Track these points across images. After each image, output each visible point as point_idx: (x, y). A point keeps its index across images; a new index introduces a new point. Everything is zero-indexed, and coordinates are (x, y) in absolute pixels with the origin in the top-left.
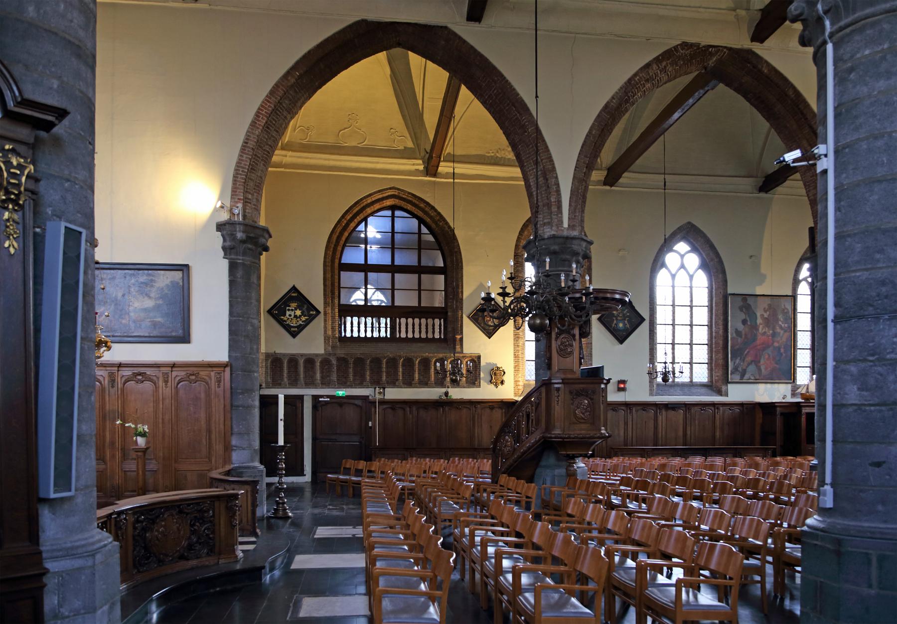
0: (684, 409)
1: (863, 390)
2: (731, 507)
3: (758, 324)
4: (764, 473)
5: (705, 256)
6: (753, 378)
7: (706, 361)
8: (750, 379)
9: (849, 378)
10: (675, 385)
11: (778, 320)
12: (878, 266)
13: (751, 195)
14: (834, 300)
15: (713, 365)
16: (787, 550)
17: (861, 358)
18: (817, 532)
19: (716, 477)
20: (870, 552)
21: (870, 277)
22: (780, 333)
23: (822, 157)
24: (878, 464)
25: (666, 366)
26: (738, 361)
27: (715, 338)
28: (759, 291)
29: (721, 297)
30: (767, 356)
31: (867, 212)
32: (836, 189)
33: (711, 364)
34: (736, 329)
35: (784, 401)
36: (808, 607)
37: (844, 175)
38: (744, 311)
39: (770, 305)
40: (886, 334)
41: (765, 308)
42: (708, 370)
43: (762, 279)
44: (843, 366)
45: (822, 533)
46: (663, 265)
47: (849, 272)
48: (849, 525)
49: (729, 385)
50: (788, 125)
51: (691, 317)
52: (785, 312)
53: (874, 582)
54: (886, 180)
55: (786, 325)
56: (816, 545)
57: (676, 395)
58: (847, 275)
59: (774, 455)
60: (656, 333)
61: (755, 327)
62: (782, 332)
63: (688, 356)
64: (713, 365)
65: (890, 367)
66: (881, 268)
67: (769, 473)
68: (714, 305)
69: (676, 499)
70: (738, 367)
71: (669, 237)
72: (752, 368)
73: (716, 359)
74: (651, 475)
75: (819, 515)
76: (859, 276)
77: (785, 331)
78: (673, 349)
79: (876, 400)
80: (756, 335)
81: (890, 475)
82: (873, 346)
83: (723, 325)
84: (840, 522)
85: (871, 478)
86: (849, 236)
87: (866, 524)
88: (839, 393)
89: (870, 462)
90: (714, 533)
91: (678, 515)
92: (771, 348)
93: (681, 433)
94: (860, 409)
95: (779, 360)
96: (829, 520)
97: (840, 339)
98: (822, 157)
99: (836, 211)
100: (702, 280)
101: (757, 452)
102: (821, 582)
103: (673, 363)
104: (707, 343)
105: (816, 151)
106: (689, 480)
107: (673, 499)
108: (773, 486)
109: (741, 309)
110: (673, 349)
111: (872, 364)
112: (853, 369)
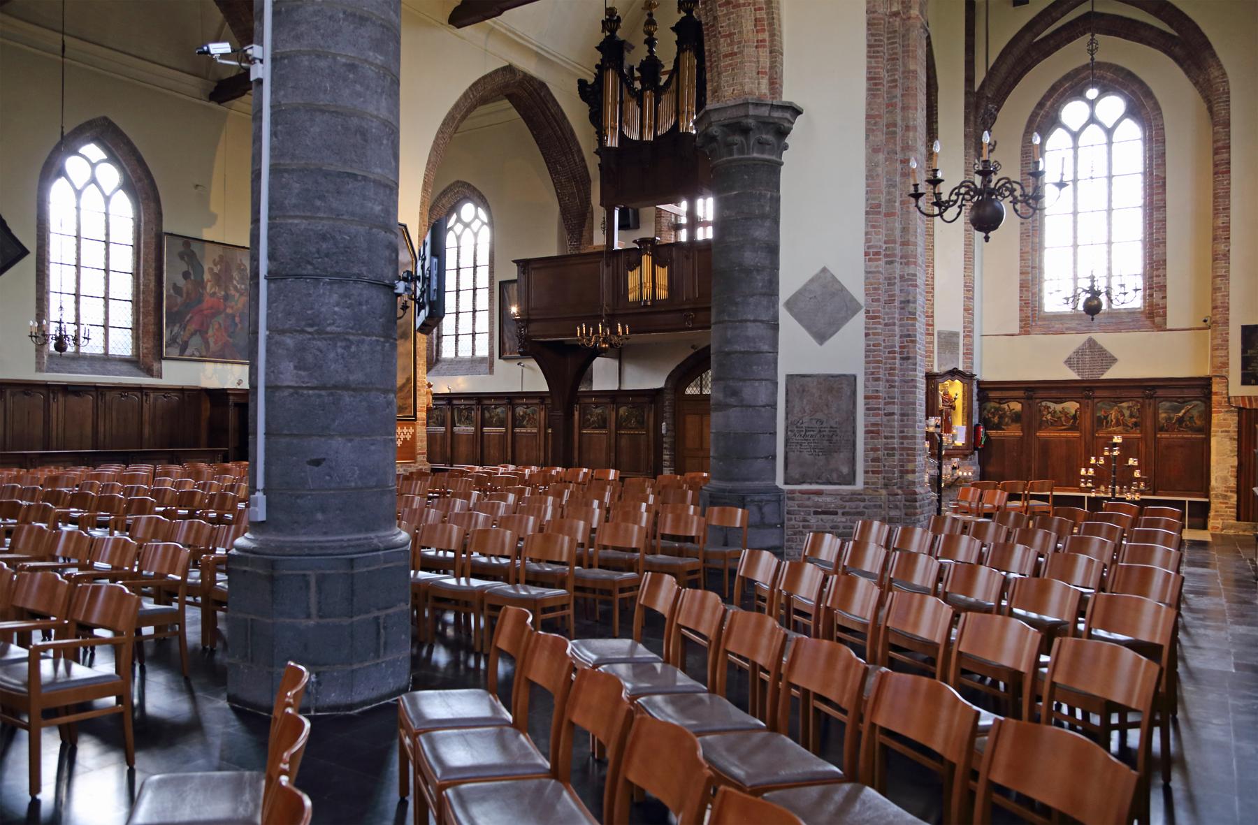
0: (94, 394)
1: (300, 369)
2: (187, 537)
3: (205, 280)
4: (205, 484)
5: (130, 174)
6: (197, 354)
7: (130, 326)
8: (193, 355)
9: (285, 352)
10: (78, 357)
11: (231, 278)
12: (318, 215)
13: (198, 101)
14: (268, 250)
15: (141, 332)
16: (218, 584)
17: (299, 329)
18: (247, 554)
19: (134, 492)
20: (308, 572)
21: (310, 227)
22: (234, 296)
23: (257, 61)
24: (317, 463)
25: (61, 328)
26: (176, 329)
27: (143, 293)
28: (207, 235)
29: (153, 235)
30: (217, 326)
31: (307, 145)
32: (272, 107)
33: (137, 330)
34: (175, 284)
35: (239, 387)
36: (237, 656)
37: (282, 93)
38: (186, 258)
39: (221, 257)
40: (327, 301)
41: (214, 260)
42: (133, 338)
43: (211, 220)
44: (277, 337)
45: (252, 556)
46: (61, 173)
47: (284, 217)
48: (284, 542)
49: (164, 363)
50: (243, 19)
51: (107, 258)
52: (241, 269)
53: (314, 611)
54: (329, 112)
55: (243, 287)
56: (245, 571)
57: (81, 373)
58: (282, 221)
59: (226, 460)
60: (48, 276)
61: (201, 284)
62: (237, 295)
63: (102, 316)
64: (141, 332)
65: (331, 343)
66: (322, 219)
67: (211, 484)
68: (142, 245)
69: (98, 533)
70: (176, 338)
71: (69, 135)
72: (196, 341)
73: (144, 323)
74: (29, 494)
75: (251, 533)
76: (297, 225)
77: (242, 294)
78: (77, 302)
79: (315, 383)
80: (202, 295)
81: (330, 476)
82: (312, 314)
83: (156, 275)
84: (274, 538)
85: (310, 480)
86: (286, 171)
87: (304, 538)
88: (273, 372)
89: (308, 459)
90: (119, 572)
91: (58, 552)
92: (223, 315)
93: (88, 429)
94: (297, 393)
95: (232, 333)
96: (261, 538)
97: (275, 302)
98: (257, 61)
99: (272, 135)
100: (124, 210)
101: (201, 456)
102: (252, 620)
103: (77, 323)
104: (131, 299)
105: (249, 52)
106: (90, 498)
107: (93, 533)
108: (214, 499)
109: (181, 256)
110: (77, 302)
111: (310, 336)
112: (289, 341)
